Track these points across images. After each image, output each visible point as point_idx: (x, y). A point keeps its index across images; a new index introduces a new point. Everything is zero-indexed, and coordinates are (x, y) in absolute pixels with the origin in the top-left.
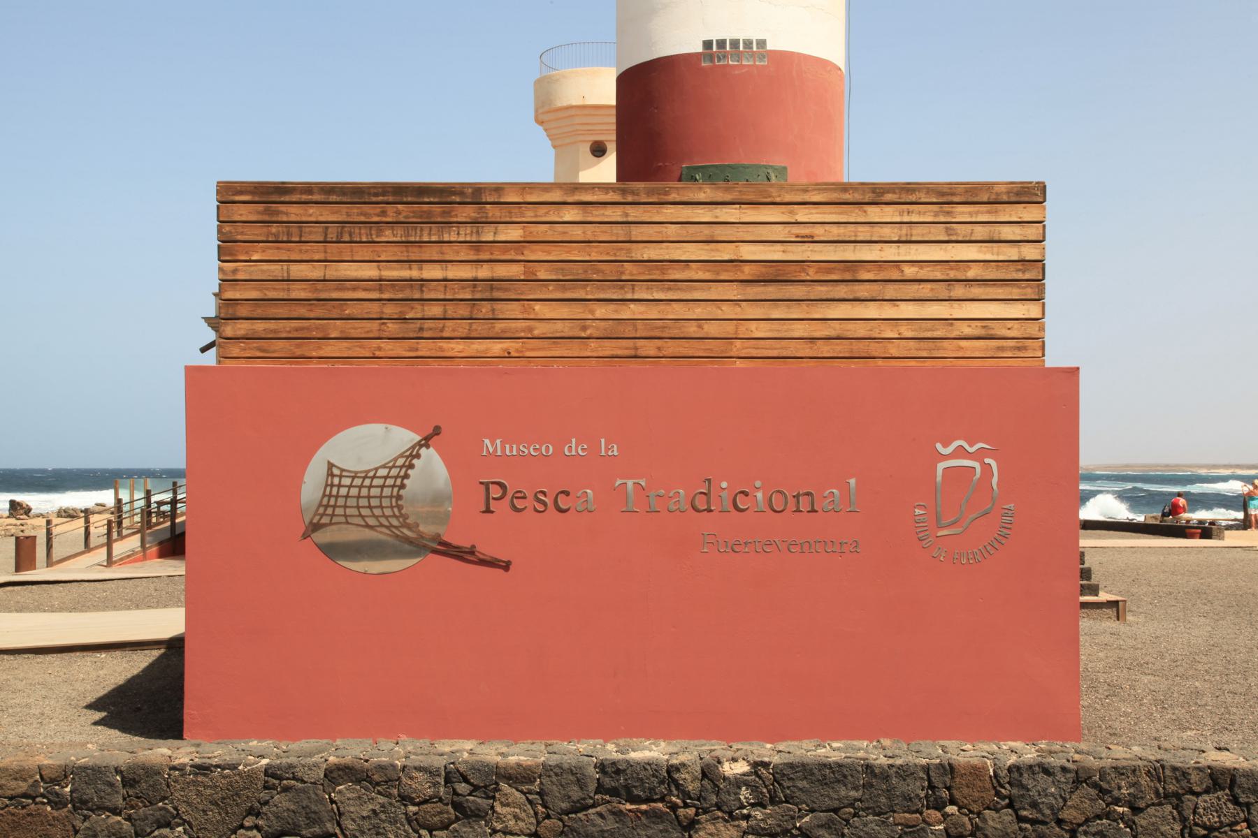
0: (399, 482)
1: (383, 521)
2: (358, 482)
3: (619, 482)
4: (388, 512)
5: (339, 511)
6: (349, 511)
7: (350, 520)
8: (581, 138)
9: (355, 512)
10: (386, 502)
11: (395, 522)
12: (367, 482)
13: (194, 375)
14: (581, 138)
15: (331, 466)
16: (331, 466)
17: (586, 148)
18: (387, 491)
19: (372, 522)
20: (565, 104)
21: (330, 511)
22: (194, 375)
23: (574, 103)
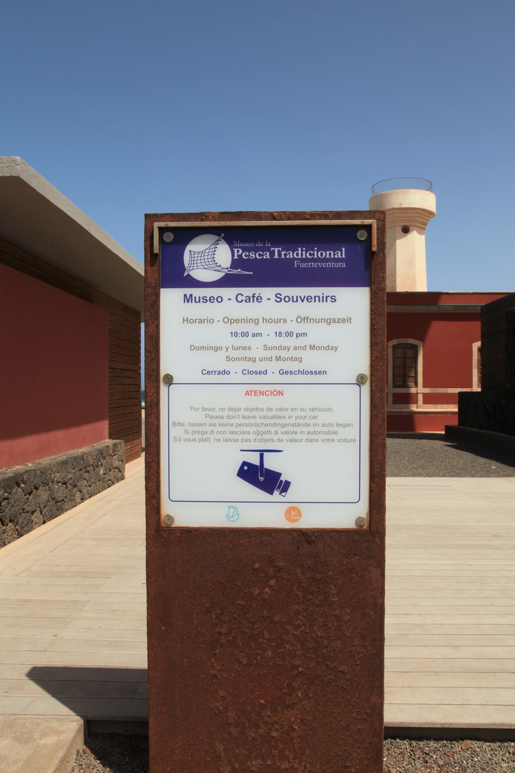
0: (213, 253)
1: (210, 266)
2: (200, 255)
3: (272, 249)
4: (211, 263)
5: (195, 265)
6: (198, 265)
7: (199, 267)
8: (397, 224)
9: (200, 264)
10: (210, 260)
11: (213, 266)
12: (203, 254)
13: (280, 474)
14: (397, 224)
15: (190, 251)
16: (190, 251)
17: (399, 229)
18: (209, 257)
19: (206, 267)
20: (391, 207)
21: (192, 265)
22: (280, 474)
23: (396, 207)
